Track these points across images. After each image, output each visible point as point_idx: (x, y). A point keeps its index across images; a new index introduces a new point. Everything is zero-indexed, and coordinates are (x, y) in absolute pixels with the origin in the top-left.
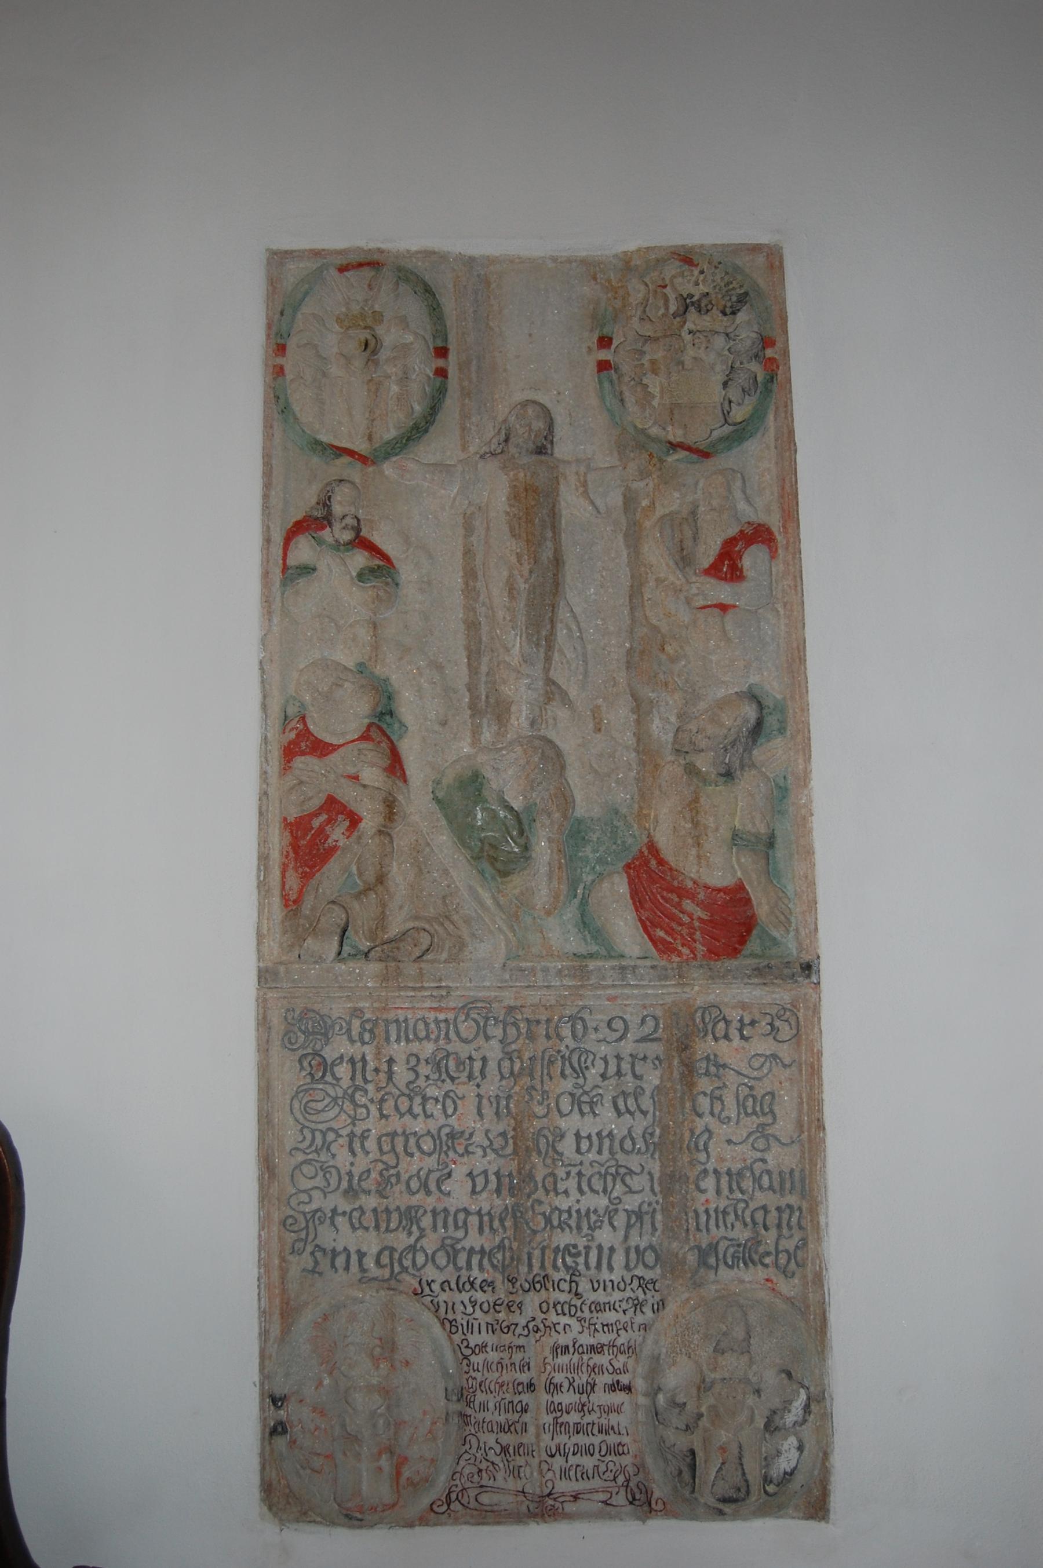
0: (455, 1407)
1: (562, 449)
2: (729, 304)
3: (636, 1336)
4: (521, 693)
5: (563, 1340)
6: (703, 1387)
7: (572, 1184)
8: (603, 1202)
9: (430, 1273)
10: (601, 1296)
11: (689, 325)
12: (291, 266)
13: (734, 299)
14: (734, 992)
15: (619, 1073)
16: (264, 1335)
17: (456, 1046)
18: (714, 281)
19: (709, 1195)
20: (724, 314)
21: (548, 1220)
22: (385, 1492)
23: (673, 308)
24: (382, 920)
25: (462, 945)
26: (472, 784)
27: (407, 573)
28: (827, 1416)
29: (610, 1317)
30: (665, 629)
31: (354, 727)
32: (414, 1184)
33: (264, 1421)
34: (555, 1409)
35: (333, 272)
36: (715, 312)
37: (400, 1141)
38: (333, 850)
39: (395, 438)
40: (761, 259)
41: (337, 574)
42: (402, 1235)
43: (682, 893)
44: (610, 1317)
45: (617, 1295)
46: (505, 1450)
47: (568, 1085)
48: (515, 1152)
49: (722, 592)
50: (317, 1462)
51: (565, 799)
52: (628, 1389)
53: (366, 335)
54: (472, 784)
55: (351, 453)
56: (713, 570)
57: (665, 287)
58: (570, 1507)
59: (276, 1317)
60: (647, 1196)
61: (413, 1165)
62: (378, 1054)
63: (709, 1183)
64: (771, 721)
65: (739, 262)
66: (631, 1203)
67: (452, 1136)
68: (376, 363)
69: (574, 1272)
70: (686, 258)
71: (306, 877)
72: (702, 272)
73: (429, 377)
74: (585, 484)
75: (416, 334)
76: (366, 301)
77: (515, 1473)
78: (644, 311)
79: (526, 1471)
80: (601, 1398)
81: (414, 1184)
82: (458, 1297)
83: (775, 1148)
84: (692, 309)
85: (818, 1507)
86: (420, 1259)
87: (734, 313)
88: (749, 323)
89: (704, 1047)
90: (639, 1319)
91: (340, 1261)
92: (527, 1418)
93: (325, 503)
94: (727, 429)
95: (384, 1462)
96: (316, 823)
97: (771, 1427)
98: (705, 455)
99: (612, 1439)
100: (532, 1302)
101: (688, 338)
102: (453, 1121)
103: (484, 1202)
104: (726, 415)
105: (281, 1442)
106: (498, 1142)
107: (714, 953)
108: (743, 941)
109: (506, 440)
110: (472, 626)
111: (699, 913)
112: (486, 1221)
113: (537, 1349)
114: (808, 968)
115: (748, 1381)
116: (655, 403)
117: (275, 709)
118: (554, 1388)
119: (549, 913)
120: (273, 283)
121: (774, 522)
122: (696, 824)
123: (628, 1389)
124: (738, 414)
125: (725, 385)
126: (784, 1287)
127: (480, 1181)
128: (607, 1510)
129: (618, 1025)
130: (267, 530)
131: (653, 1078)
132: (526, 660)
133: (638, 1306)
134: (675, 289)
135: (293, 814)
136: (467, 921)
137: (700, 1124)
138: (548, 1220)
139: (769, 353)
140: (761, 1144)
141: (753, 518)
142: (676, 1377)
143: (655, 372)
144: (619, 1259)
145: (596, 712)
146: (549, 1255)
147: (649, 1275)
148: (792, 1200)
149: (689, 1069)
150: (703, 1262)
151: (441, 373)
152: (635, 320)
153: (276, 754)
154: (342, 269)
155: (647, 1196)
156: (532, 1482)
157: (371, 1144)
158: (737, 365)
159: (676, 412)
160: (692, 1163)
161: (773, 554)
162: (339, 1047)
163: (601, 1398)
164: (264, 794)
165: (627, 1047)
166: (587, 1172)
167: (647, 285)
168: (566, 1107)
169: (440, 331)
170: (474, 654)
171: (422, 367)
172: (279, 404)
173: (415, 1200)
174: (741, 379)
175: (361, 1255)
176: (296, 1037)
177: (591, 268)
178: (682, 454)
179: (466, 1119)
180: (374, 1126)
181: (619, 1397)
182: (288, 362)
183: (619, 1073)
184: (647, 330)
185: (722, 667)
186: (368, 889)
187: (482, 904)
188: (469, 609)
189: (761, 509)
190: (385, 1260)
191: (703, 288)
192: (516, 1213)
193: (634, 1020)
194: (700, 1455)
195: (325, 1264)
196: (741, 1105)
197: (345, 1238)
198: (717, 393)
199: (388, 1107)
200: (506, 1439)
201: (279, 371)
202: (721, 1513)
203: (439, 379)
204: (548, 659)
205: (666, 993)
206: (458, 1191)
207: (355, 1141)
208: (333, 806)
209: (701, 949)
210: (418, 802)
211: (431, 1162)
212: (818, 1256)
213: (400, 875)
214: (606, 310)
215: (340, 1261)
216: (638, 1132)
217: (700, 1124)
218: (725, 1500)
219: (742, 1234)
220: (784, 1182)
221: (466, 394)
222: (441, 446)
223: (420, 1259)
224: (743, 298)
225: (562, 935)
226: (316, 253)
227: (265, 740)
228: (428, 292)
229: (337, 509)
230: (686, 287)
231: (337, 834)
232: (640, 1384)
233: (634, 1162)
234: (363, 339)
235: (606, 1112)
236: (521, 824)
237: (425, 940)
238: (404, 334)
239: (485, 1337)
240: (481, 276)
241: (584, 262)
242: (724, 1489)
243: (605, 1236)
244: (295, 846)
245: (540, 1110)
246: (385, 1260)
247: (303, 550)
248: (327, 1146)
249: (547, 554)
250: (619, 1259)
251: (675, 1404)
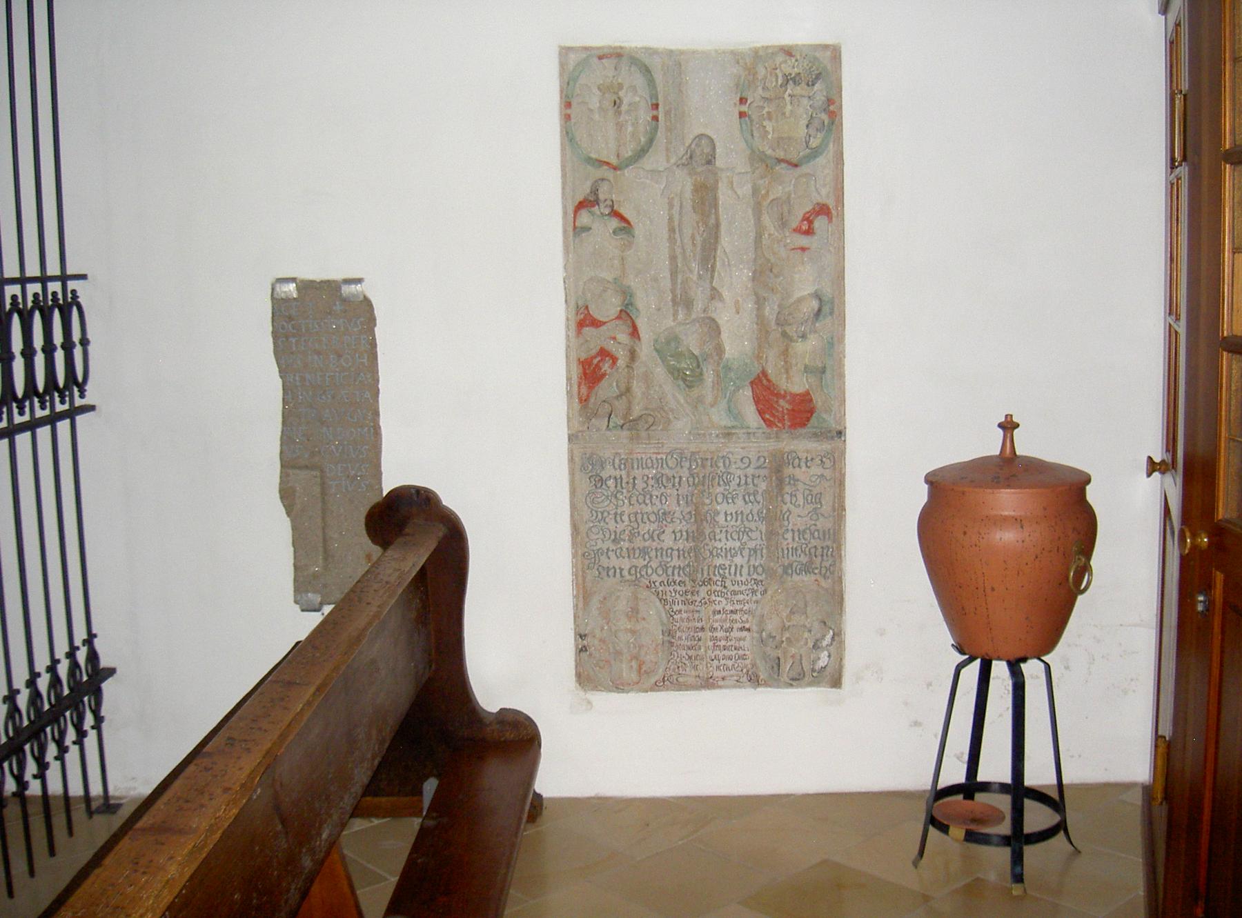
0: (666, 638)
1: (719, 163)
3: (754, 606)
4: (699, 296)
5: (718, 608)
6: (784, 629)
7: (723, 535)
8: (738, 544)
9: (654, 577)
10: (736, 588)
11: (789, 91)
12: (572, 56)
14: (802, 445)
15: (746, 483)
16: (576, 606)
17: (666, 471)
19: (789, 541)
21: (711, 553)
22: (634, 676)
23: (780, 82)
24: (629, 409)
25: (669, 422)
26: (673, 339)
27: (639, 230)
28: (842, 643)
29: (741, 597)
30: (773, 260)
31: (614, 311)
32: (646, 536)
33: (577, 646)
34: (714, 639)
35: (595, 60)
36: (803, 84)
37: (639, 516)
38: (604, 375)
40: (828, 53)
41: (602, 229)
42: (641, 560)
43: (778, 395)
44: (741, 597)
45: (744, 587)
46: (690, 658)
47: (720, 489)
48: (696, 521)
49: (803, 241)
50: (601, 664)
51: (720, 350)
52: (749, 630)
53: (615, 97)
54: (673, 339)
55: (608, 164)
56: (798, 230)
58: (721, 683)
59: (581, 598)
60: (759, 542)
61: (646, 528)
62: (628, 476)
63: (789, 536)
64: (826, 309)
66: (752, 545)
67: (664, 514)
68: (620, 113)
69: (724, 577)
70: (788, 52)
71: (591, 388)
74: (732, 183)
77: (695, 668)
79: (700, 667)
80: (735, 634)
81: (646, 536)
82: (668, 589)
83: (821, 519)
85: (836, 683)
86: (650, 571)
89: (789, 471)
90: (754, 598)
91: (611, 573)
92: (700, 643)
93: (595, 191)
94: (808, 151)
95: (634, 663)
96: (595, 361)
97: (816, 646)
98: (796, 166)
99: (741, 652)
100: (703, 591)
101: (788, 99)
102: (665, 507)
103: (681, 544)
104: (807, 143)
105: (583, 654)
106: (687, 517)
107: (794, 426)
108: (808, 419)
109: (691, 157)
110: (673, 258)
111: (787, 406)
112: (681, 554)
113: (705, 612)
114: (840, 433)
115: (804, 626)
117: (572, 304)
118: (713, 629)
119: (712, 406)
120: (562, 65)
121: (831, 203)
122: (786, 362)
123: (749, 630)
124: (814, 143)
126: (823, 583)
127: (678, 535)
128: (738, 684)
129: (746, 460)
130: (564, 207)
131: (763, 486)
132: (700, 277)
133: (754, 592)
135: (583, 356)
136: (672, 410)
137: (785, 508)
138: (711, 553)
139: (831, 108)
140: (815, 517)
141: (820, 201)
142: (772, 626)
143: (770, 119)
144: (745, 571)
145: (737, 302)
146: (712, 569)
147: (760, 578)
148: (829, 543)
149: (781, 483)
150: (785, 572)
151: (655, 118)
152: (760, 89)
153: (573, 326)
154: (600, 58)
155: (759, 542)
156: (702, 670)
157: (625, 518)
160: (781, 527)
161: (830, 219)
162: (608, 471)
163: (735, 634)
164: (568, 347)
165: (750, 471)
166: (730, 530)
168: (720, 500)
169: (654, 95)
170: (674, 273)
171: (645, 116)
172: (569, 136)
173: (647, 544)
174: (816, 123)
175: (621, 570)
176: (588, 471)
177: (736, 56)
178: (783, 165)
179: (671, 505)
180: (627, 509)
181: (745, 633)
182: (573, 112)
183: (746, 483)
184: (767, 95)
185: (804, 282)
186: (621, 395)
187: (678, 402)
188: (672, 249)
189: (824, 195)
190: (633, 572)
192: (696, 550)
193: (754, 460)
194: (782, 661)
195: (604, 574)
196: (805, 499)
197: (614, 562)
198: (802, 131)
199: (634, 500)
200: (690, 653)
201: (567, 118)
202: (791, 685)
204: (712, 277)
205: (771, 445)
206: (668, 541)
207: (617, 517)
208: (604, 353)
209: (788, 423)
210: (645, 349)
211: (653, 527)
212: (841, 570)
213: (638, 388)
215: (611, 573)
216: (755, 512)
217: (785, 508)
218: (793, 679)
219: (804, 559)
220: (825, 534)
221: (669, 130)
222: (656, 160)
223: (650, 571)
224: (818, 76)
225: (719, 417)
226: (586, 49)
227: (568, 319)
228: (646, 71)
229: (602, 197)
230: (787, 69)
231: (606, 367)
232: (754, 628)
233: (753, 525)
235: (740, 502)
236: (698, 362)
237: (651, 420)
238: (635, 96)
239: (681, 607)
240: (677, 62)
241: (733, 53)
242: (793, 674)
243: (738, 560)
244: (585, 374)
245: (707, 501)
246: (633, 572)
247: (585, 218)
248: (604, 519)
249: (712, 221)
250: (745, 571)
251: (770, 636)
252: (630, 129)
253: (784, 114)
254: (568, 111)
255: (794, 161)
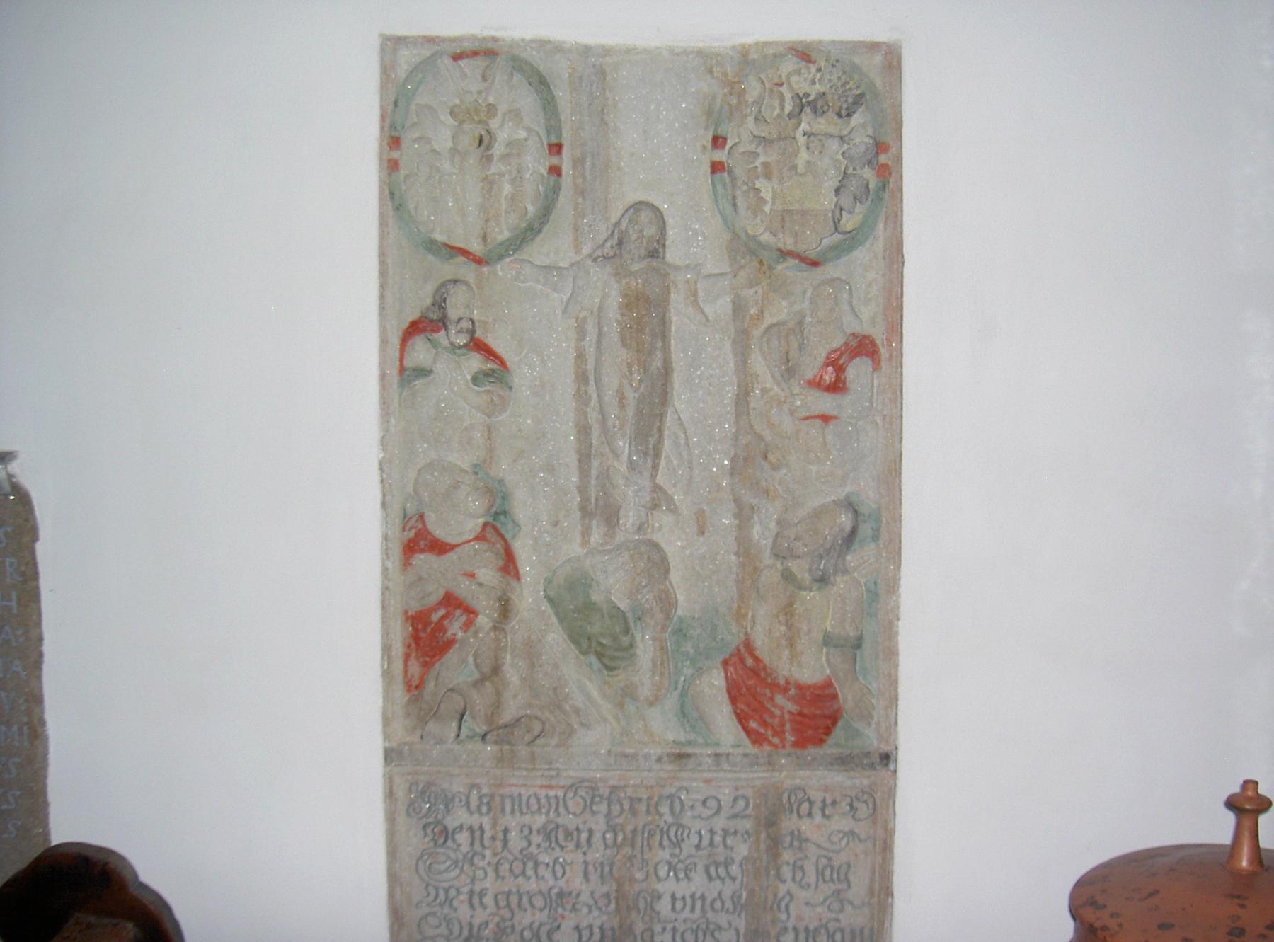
2: (845, 106)
13: (850, 100)
18: (830, 80)
20: (840, 115)
23: (788, 108)
35: (447, 61)
39: (508, 240)
40: (878, 58)
57: (781, 85)
65: (857, 60)
68: (489, 159)
70: (804, 53)
72: (819, 70)
73: (543, 176)
75: (529, 130)
76: (480, 92)
78: (760, 111)
84: (808, 109)
87: (849, 115)
88: (864, 126)
98: (815, 264)
101: (802, 140)
104: (836, 223)
116: (767, 209)
125: (837, 191)
134: (791, 88)
139: (883, 159)
143: (768, 176)
151: (555, 171)
158: (850, 171)
159: (787, 219)
167: (763, 82)
174: (853, 185)
178: (792, 262)
182: (405, 156)
191: (818, 88)
198: (827, 201)
203: (553, 178)
214: (721, 107)
224: (858, 100)
230: (802, 86)
234: (477, 135)
252: (507, 189)
253: (794, 167)
254: (395, 155)
255: (812, 255)
